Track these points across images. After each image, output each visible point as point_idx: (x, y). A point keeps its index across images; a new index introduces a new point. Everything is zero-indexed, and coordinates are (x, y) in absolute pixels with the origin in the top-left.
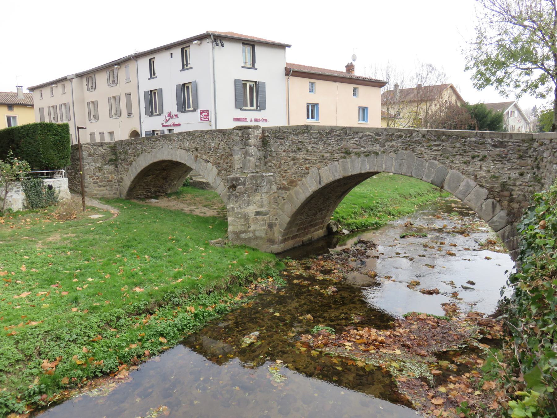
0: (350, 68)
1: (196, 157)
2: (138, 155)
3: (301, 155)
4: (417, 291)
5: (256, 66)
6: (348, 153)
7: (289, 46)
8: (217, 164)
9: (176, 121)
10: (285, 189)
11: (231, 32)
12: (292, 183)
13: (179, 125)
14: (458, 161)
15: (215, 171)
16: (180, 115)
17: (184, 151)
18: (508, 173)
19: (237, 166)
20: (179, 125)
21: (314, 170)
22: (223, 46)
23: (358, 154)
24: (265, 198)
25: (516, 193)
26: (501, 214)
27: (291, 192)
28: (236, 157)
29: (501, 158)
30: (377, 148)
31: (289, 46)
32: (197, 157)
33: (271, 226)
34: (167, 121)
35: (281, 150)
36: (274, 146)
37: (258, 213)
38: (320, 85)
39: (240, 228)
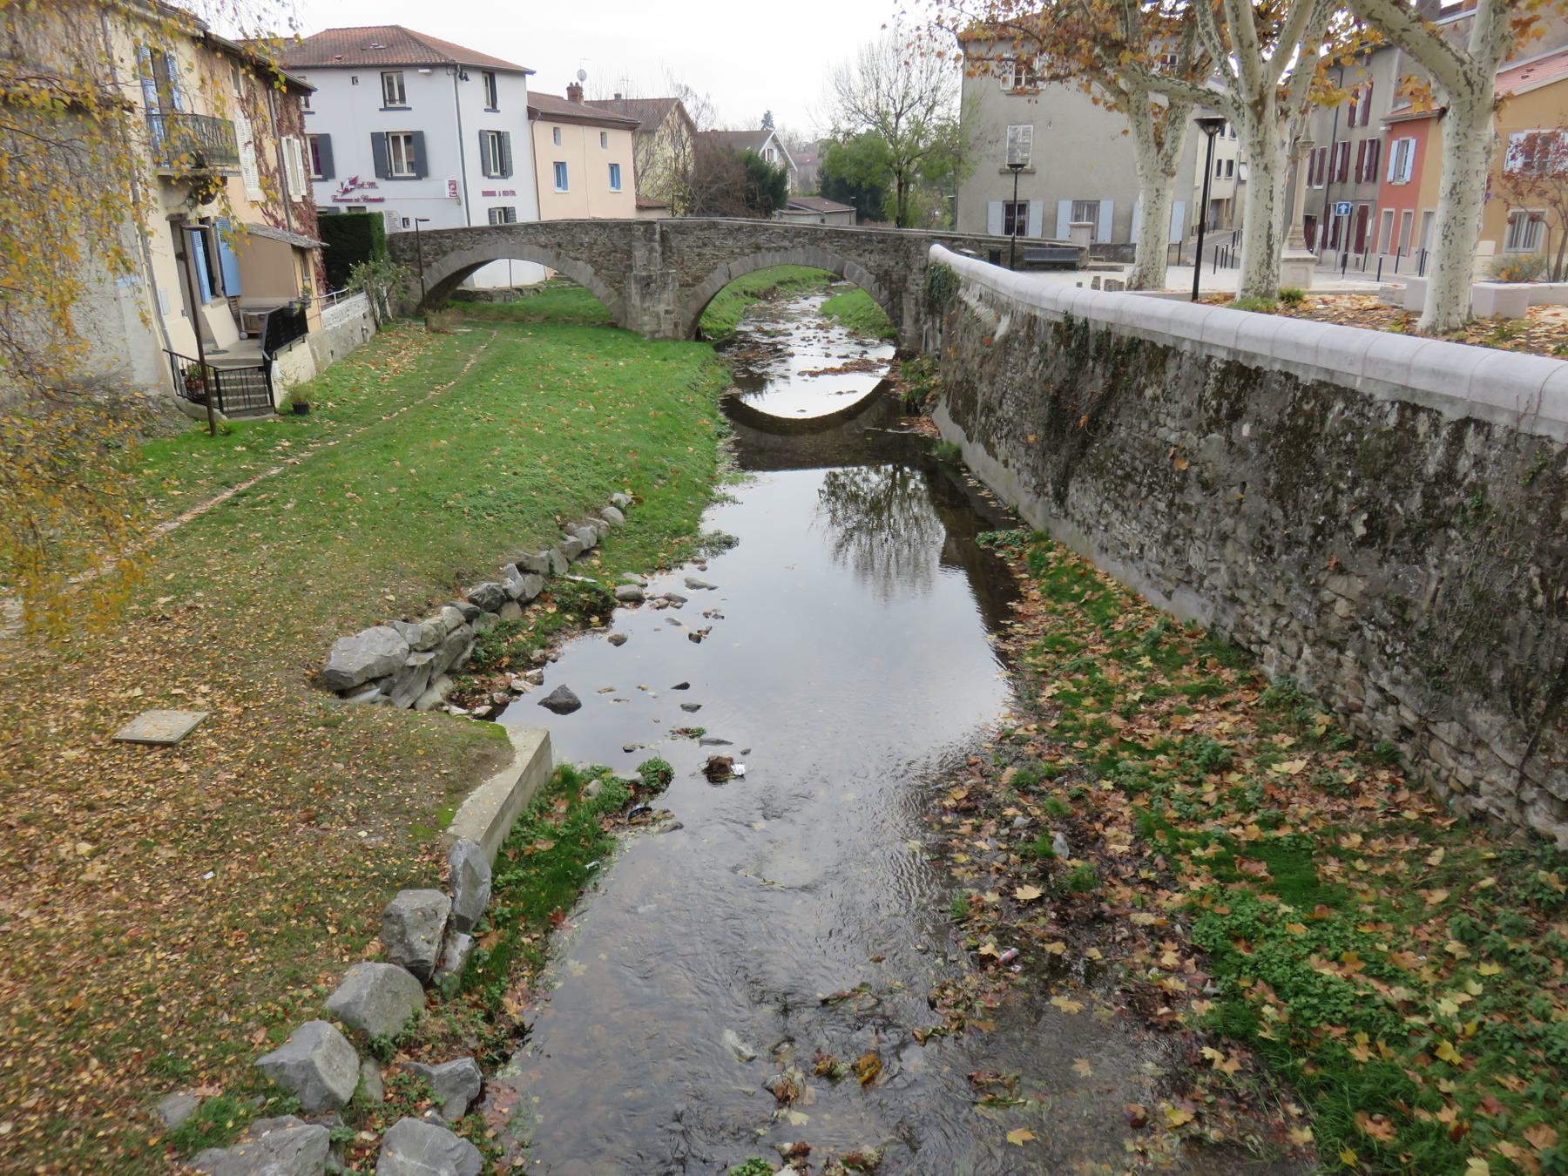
0: (575, 92)
1: (559, 254)
2: (445, 253)
3: (708, 251)
4: (652, 598)
5: (499, 107)
6: (758, 248)
7: (532, 73)
8: (593, 262)
9: (372, 194)
10: (688, 285)
11: (397, 28)
12: (698, 279)
13: (381, 200)
14: (853, 254)
15: (590, 269)
16: (382, 183)
17: (536, 248)
18: (889, 262)
19: (639, 263)
20: (381, 200)
21: (722, 265)
22: (1086, 321)
23: (769, 250)
24: (671, 296)
25: (894, 277)
26: (885, 293)
27: (698, 288)
28: (637, 254)
29: (884, 251)
30: (786, 243)
31: (532, 73)
32: (559, 254)
33: (676, 325)
34: (346, 191)
35: (684, 246)
36: (675, 241)
37: (667, 312)
38: (567, 130)
39: (654, 327)
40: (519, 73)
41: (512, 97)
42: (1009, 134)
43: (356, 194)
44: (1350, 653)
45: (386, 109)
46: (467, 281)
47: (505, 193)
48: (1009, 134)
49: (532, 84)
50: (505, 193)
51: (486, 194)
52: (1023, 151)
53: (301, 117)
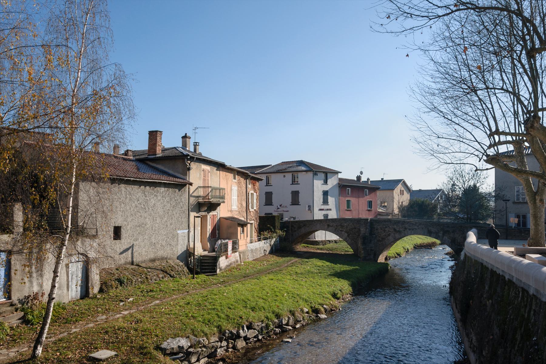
0: (359, 178)
3: (387, 229)
7: (341, 173)
23: (410, 229)
30: (416, 227)
31: (341, 173)
40: (337, 173)
41: (333, 182)
42: (516, 189)
43: (281, 209)
44: (34, 267)
45: (292, 184)
46: (311, 236)
47: (328, 210)
48: (516, 189)
49: (340, 176)
50: (328, 210)
51: (320, 210)
52: (523, 195)
53: (531, 98)
